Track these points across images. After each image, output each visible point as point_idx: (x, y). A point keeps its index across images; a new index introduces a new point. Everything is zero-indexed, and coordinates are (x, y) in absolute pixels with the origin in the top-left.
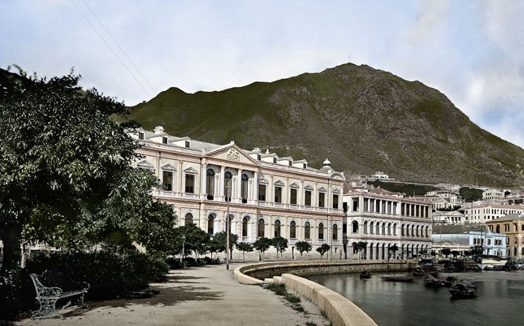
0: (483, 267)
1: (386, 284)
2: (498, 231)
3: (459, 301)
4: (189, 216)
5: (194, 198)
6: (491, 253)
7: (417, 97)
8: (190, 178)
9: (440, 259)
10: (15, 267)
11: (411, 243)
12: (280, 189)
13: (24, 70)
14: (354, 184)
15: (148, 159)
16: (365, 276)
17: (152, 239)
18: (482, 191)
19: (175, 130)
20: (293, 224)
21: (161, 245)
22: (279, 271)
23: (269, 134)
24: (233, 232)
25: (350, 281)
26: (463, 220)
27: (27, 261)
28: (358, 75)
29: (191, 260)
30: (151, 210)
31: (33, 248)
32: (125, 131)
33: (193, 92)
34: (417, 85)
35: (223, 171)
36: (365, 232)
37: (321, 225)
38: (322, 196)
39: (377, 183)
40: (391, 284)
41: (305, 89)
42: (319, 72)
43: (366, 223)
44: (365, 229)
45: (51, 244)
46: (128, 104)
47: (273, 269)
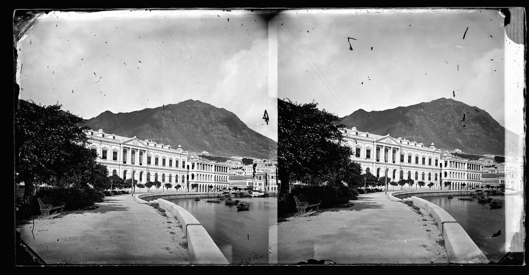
0: (253, 196)
1: (460, 201)
2: (260, 179)
3: (241, 212)
4: (115, 171)
5: (117, 163)
6: (257, 189)
7: (222, 116)
8: (115, 153)
9: (233, 192)
10: (287, 192)
11: (472, 182)
12: (411, 157)
13: (291, 100)
14: (445, 155)
15: (349, 142)
16: (450, 197)
17: (351, 180)
18: (253, 160)
19: (362, 128)
20: (164, 175)
21: (101, 185)
22: (155, 197)
23: (153, 133)
24: (389, 177)
25: (443, 200)
26: (496, 172)
27: (292, 190)
28: (195, 105)
29: (369, 189)
30: (96, 168)
31: (295, 184)
32: (83, 131)
33: (370, 111)
34: (222, 110)
35: (131, 150)
36: (450, 177)
37: (430, 174)
38: (430, 160)
39: (456, 154)
40: (463, 201)
41: (169, 112)
42: (176, 103)
43: (198, 175)
44: (450, 176)
45: (303, 182)
46: (340, 116)
47: (407, 194)
